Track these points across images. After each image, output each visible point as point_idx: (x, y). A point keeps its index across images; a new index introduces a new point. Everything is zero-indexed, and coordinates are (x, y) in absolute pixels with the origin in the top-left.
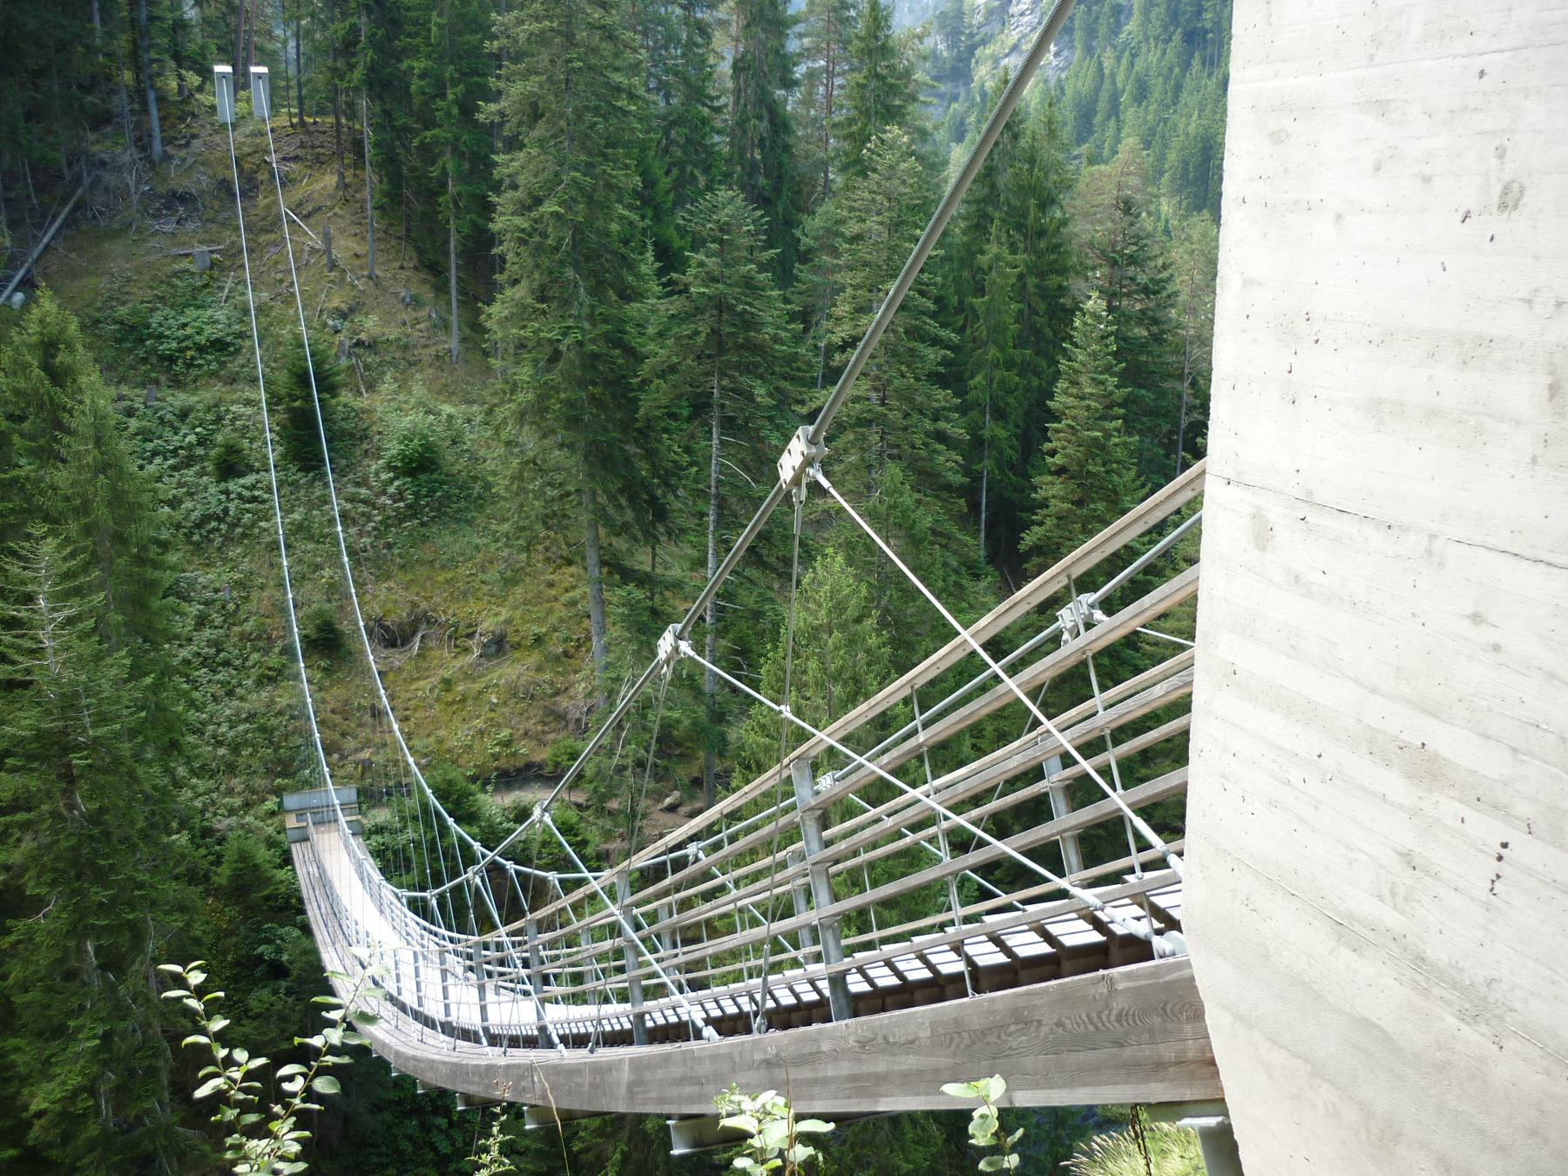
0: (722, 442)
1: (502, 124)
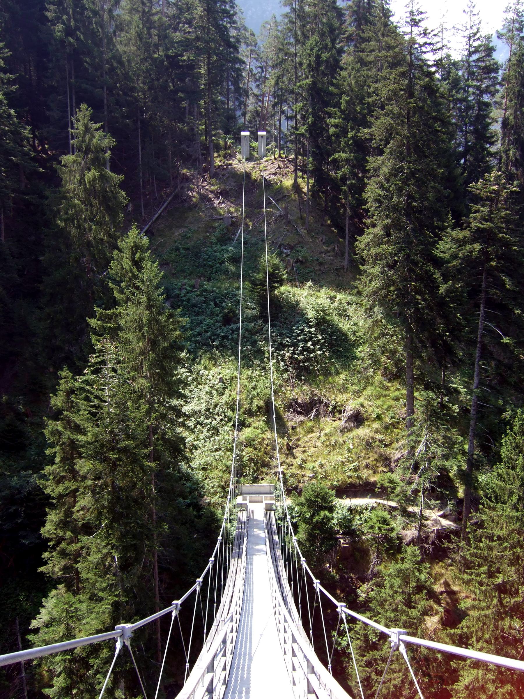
0: (485, 312)
1: (372, 140)
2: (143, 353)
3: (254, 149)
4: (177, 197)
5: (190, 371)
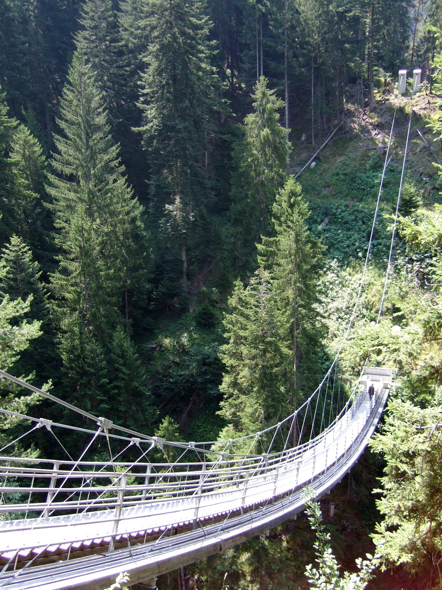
2: (291, 272)
3: (410, 84)
4: (341, 129)
5: (338, 276)
